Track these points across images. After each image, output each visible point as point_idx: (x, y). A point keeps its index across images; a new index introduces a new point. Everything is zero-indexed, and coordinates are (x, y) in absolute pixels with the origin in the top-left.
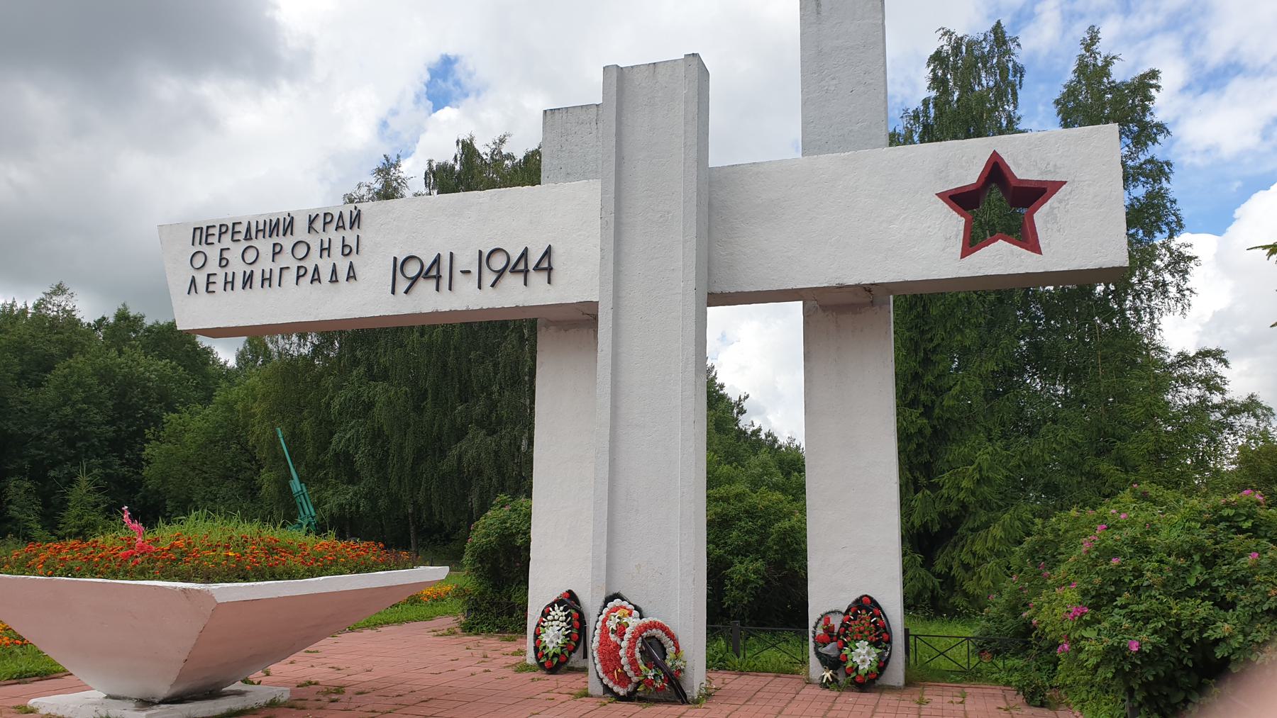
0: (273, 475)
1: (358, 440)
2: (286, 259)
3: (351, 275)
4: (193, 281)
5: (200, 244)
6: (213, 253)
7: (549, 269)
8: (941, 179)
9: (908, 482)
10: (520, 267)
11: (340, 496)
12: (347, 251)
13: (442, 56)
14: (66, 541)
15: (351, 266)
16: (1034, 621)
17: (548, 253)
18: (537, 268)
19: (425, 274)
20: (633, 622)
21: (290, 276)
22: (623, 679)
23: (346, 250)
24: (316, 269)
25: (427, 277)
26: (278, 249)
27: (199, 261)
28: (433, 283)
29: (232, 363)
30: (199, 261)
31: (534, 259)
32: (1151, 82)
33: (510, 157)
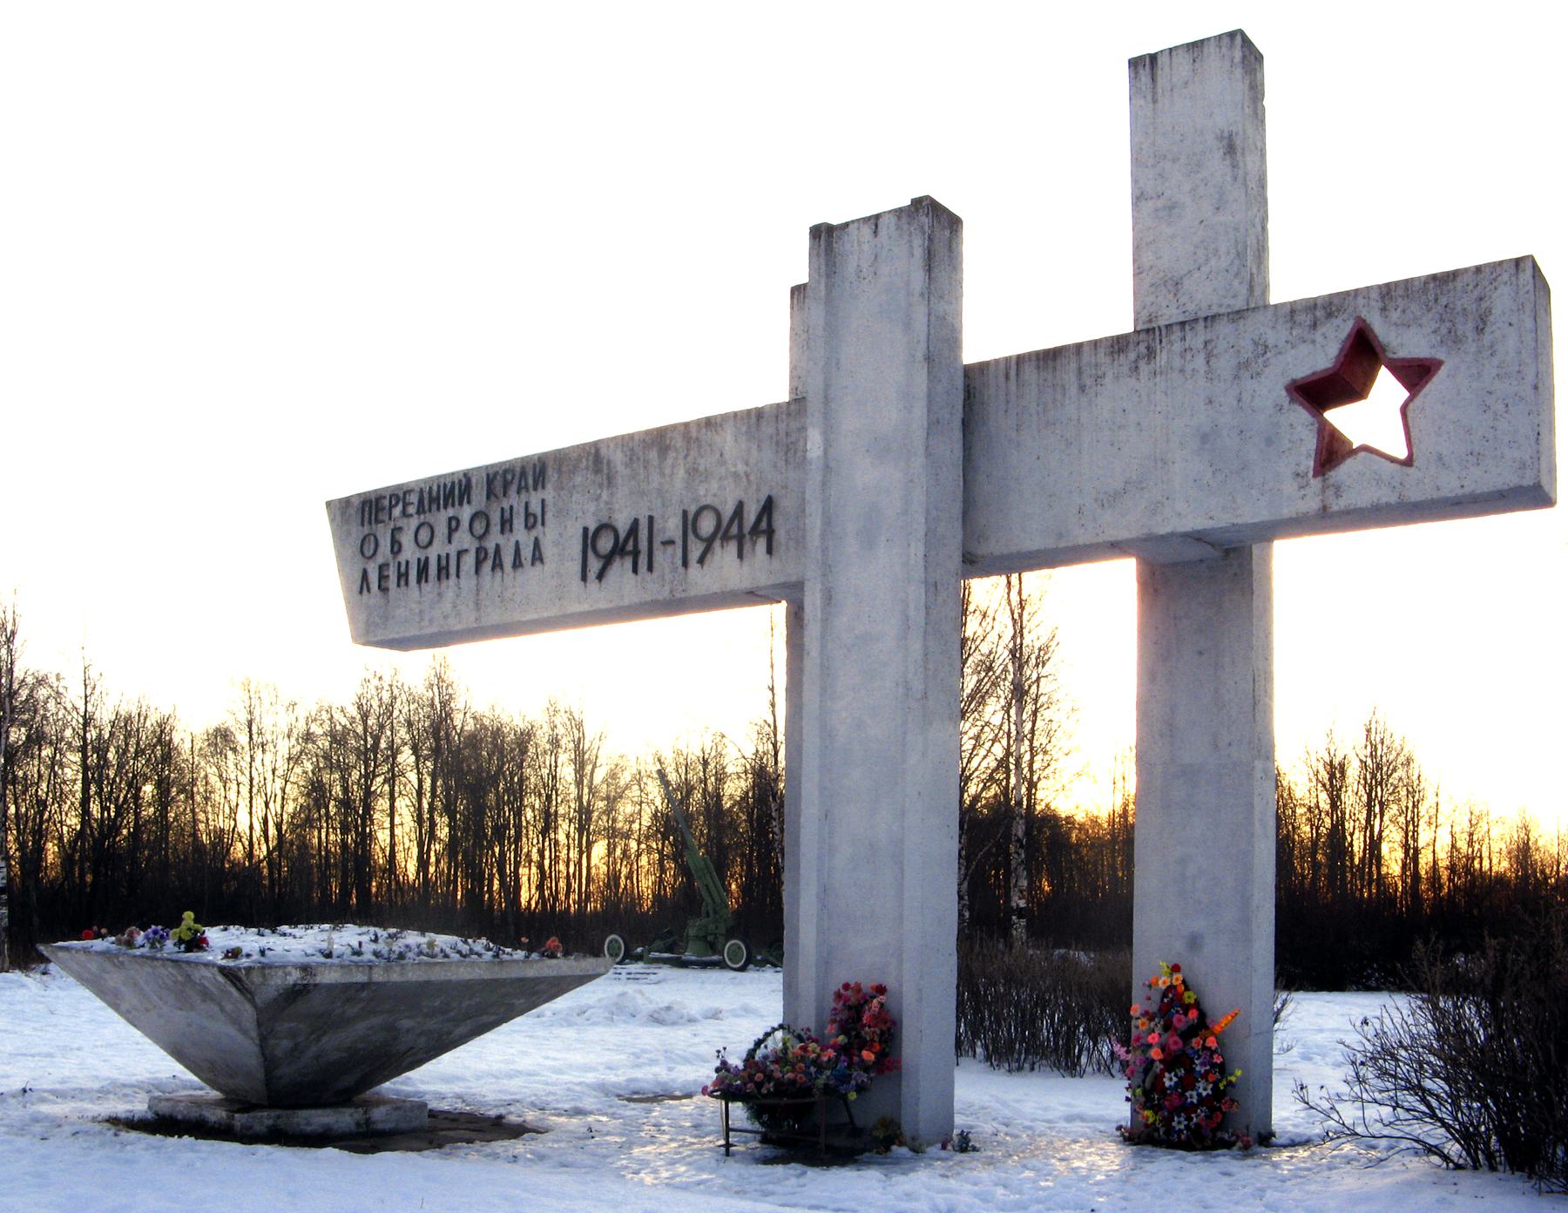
2: (463, 539)
3: (538, 557)
5: (448, 555)
7: (770, 533)
8: (1151, 267)
13: (1556, 502)
15: (536, 539)
17: (768, 507)
18: (755, 530)
19: (618, 550)
21: (469, 561)
23: (531, 522)
24: (498, 549)
25: (726, 538)
26: (454, 524)
28: (628, 562)
29: (784, 604)
31: (751, 516)
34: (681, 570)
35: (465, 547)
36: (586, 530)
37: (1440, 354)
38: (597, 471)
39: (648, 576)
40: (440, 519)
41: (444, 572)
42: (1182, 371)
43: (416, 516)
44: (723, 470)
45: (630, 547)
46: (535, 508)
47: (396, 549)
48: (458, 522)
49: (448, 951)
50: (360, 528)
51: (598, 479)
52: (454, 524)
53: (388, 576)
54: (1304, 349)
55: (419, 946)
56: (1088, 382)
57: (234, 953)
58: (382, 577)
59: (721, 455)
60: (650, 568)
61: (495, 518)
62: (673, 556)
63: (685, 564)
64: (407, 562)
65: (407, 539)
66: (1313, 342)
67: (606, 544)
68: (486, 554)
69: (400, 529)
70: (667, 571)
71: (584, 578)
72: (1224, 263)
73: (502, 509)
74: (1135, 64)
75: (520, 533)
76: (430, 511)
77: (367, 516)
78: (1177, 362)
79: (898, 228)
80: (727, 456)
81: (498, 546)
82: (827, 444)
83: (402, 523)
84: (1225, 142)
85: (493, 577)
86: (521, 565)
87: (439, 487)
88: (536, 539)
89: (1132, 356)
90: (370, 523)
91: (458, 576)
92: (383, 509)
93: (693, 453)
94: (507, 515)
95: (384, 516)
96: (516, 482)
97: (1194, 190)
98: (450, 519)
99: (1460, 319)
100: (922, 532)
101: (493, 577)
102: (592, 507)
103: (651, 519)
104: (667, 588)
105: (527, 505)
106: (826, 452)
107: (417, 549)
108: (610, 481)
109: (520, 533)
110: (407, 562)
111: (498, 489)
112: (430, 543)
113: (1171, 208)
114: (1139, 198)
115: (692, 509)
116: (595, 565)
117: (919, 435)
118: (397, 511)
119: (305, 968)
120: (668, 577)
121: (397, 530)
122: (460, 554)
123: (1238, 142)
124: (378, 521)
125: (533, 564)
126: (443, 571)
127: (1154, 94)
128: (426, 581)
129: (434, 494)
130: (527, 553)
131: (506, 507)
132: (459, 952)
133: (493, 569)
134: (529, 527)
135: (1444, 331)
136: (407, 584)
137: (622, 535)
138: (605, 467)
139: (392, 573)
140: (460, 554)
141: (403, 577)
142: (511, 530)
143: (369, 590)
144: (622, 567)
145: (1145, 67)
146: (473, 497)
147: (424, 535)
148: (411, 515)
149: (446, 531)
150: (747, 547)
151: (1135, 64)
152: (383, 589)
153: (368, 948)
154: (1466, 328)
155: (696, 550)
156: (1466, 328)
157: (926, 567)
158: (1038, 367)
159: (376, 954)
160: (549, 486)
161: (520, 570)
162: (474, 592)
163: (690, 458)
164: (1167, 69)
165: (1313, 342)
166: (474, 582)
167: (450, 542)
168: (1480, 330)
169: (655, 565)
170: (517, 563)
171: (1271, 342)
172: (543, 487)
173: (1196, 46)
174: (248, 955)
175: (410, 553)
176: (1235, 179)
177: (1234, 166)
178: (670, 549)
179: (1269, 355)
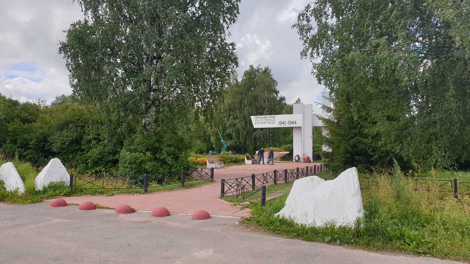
0: (214, 138)
1: (233, 131)
2: (266, 121)
6: (258, 120)
10: (293, 123)
11: (229, 143)
14: (350, 145)
20: (306, 156)
21: (267, 123)
22: (306, 161)
27: (256, 121)
30: (256, 121)
31: (294, 122)
33: (261, 69)
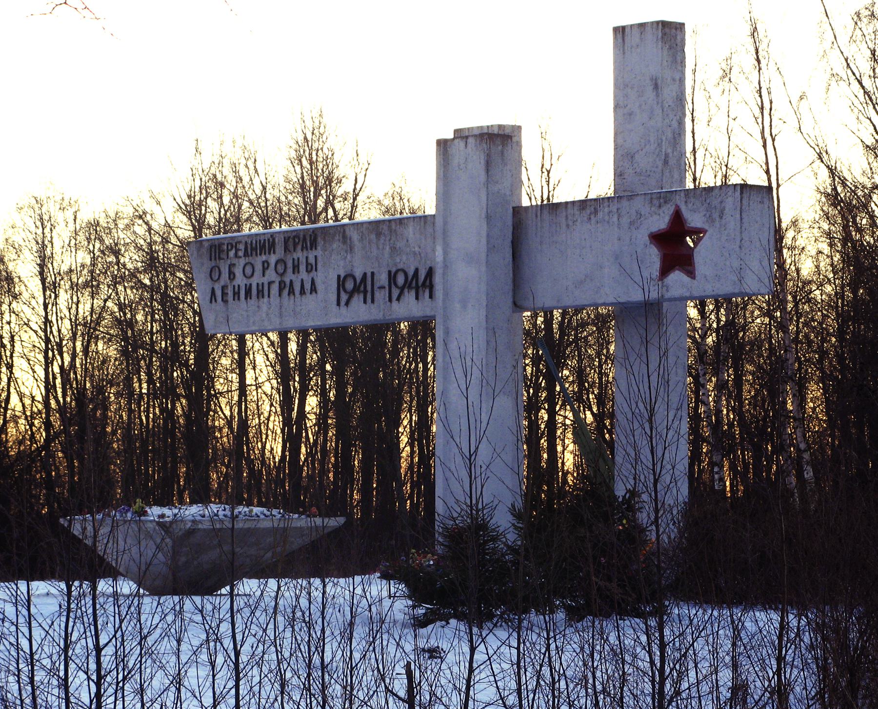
3: (314, 289)
4: (213, 291)
5: (263, 283)
7: (431, 287)
9: (100, 317)
12: (309, 269)
15: (313, 279)
16: (629, 487)
19: (356, 289)
21: (275, 288)
23: (310, 268)
25: (410, 287)
26: (266, 265)
32: (666, 541)
34: (389, 303)
35: (273, 279)
36: (339, 276)
37: (706, 227)
38: (344, 242)
39: (372, 306)
40: (258, 261)
41: (261, 293)
42: (608, 222)
43: (243, 258)
44: (408, 249)
45: (362, 288)
46: (312, 260)
47: (232, 277)
48: (268, 264)
49: (259, 514)
50: (210, 262)
51: (345, 247)
52: (266, 265)
53: (227, 293)
54: (656, 217)
55: (245, 512)
56: (571, 223)
57: (162, 516)
58: (224, 294)
59: (407, 241)
60: (373, 301)
61: (290, 264)
62: (385, 295)
63: (390, 300)
64: (239, 286)
65: (238, 271)
66: (659, 215)
67: (350, 285)
68: (285, 284)
69: (234, 265)
70: (381, 304)
71: (338, 304)
72: (653, 147)
73: (293, 259)
74: (616, 30)
75: (303, 274)
76: (252, 255)
77: (213, 254)
78: (607, 218)
79: (476, 146)
80: (410, 241)
81: (291, 281)
82: (445, 253)
83: (235, 261)
84: (654, 82)
85: (289, 299)
86: (304, 293)
87: (256, 242)
88: (313, 279)
89: (588, 212)
90: (215, 259)
91: (269, 296)
92: (224, 251)
93: (393, 238)
94: (296, 262)
95: (224, 256)
96: (301, 243)
97: (640, 106)
98: (263, 262)
99: (714, 211)
100: (485, 304)
101: (289, 299)
102: (342, 263)
103: (373, 274)
104: (381, 313)
105: (307, 258)
106: (444, 258)
107: (245, 279)
108: (351, 249)
109: (303, 274)
110: (239, 286)
111: (291, 247)
112: (252, 275)
113: (630, 114)
114: (617, 107)
115: (394, 270)
116: (344, 297)
117: (483, 256)
118: (232, 253)
119: (194, 522)
120: (382, 307)
121: (232, 266)
122: (270, 283)
123: (659, 82)
124: (220, 258)
125: (311, 293)
126: (260, 293)
127: (624, 50)
128: (251, 298)
129: (254, 245)
130: (308, 286)
131: (296, 258)
132: (265, 515)
133: (289, 295)
134: (308, 271)
135: (708, 215)
136: (239, 299)
137: (358, 281)
138: (348, 241)
139: (230, 291)
140: (270, 283)
141: (236, 294)
142: (298, 272)
143: (216, 301)
144: (357, 300)
145: (620, 32)
146: (277, 250)
147: (248, 270)
148: (241, 257)
149: (261, 268)
150: (421, 292)
151: (616, 30)
152: (225, 301)
153: (221, 513)
154: (716, 215)
155: (395, 292)
156: (716, 215)
157: (487, 322)
158: (549, 212)
159: (225, 516)
160: (319, 248)
161: (304, 296)
162: (279, 307)
163: (391, 242)
164: (630, 36)
165: (659, 215)
166: (278, 300)
167: (264, 275)
168: (721, 217)
169: (376, 299)
170: (303, 292)
171: (643, 213)
172: (316, 249)
173: (642, 26)
174: (168, 517)
175: (240, 280)
176: (658, 103)
177: (657, 95)
178: (383, 290)
179: (642, 219)
